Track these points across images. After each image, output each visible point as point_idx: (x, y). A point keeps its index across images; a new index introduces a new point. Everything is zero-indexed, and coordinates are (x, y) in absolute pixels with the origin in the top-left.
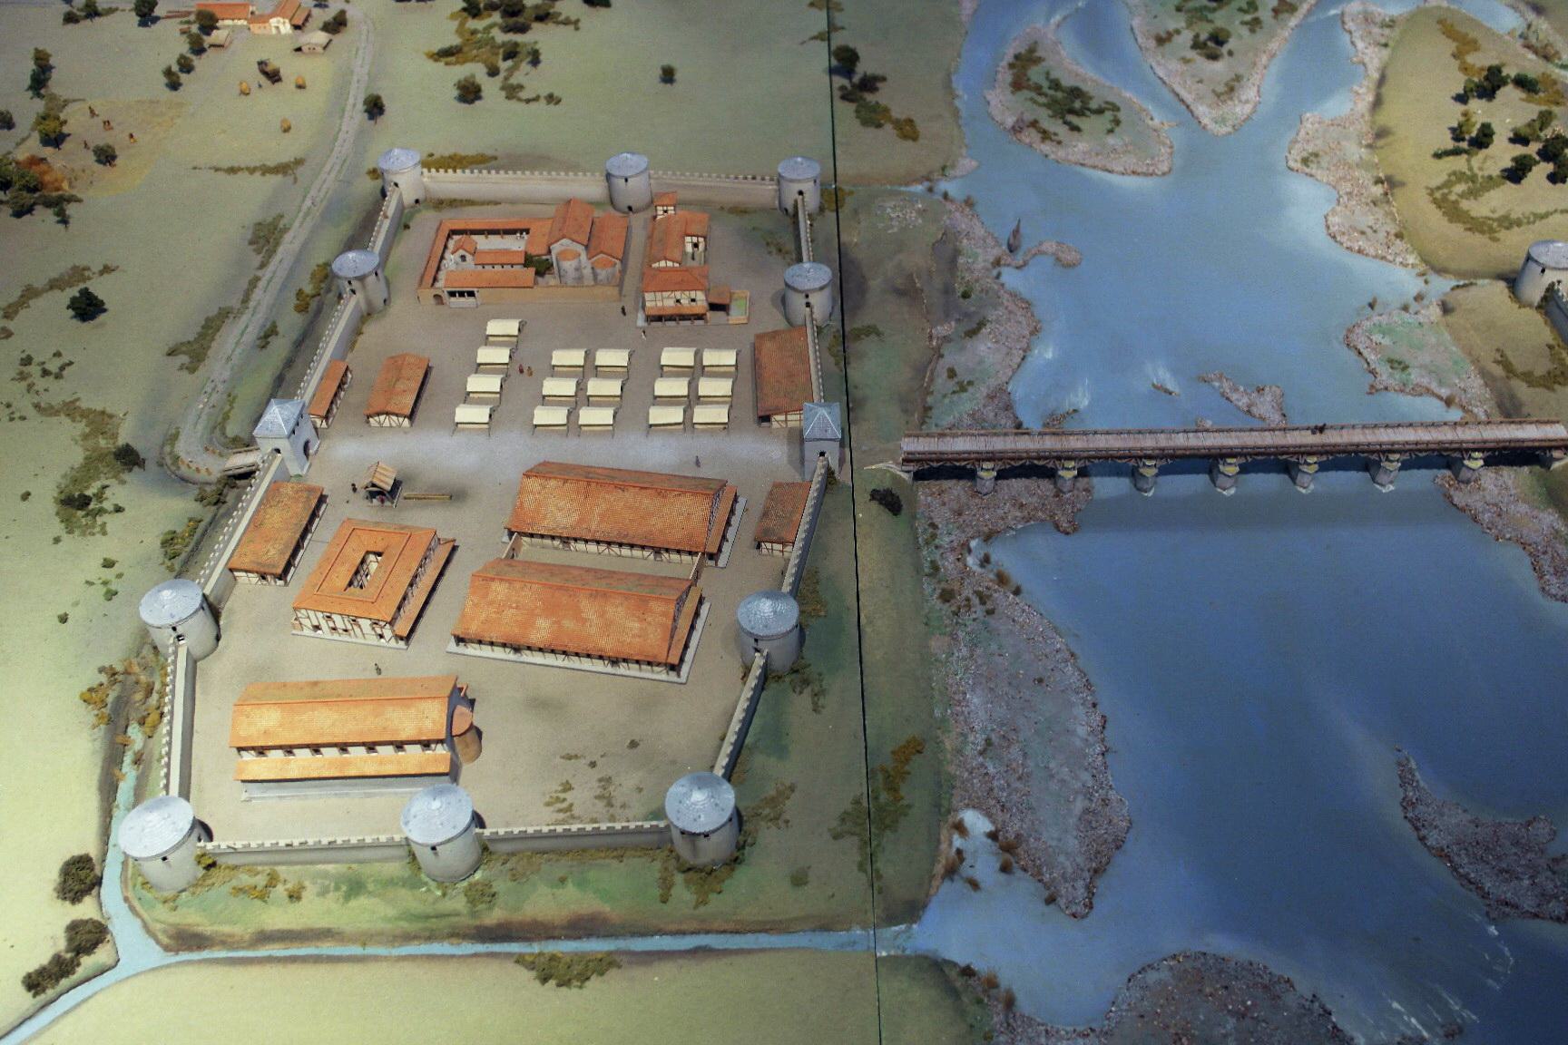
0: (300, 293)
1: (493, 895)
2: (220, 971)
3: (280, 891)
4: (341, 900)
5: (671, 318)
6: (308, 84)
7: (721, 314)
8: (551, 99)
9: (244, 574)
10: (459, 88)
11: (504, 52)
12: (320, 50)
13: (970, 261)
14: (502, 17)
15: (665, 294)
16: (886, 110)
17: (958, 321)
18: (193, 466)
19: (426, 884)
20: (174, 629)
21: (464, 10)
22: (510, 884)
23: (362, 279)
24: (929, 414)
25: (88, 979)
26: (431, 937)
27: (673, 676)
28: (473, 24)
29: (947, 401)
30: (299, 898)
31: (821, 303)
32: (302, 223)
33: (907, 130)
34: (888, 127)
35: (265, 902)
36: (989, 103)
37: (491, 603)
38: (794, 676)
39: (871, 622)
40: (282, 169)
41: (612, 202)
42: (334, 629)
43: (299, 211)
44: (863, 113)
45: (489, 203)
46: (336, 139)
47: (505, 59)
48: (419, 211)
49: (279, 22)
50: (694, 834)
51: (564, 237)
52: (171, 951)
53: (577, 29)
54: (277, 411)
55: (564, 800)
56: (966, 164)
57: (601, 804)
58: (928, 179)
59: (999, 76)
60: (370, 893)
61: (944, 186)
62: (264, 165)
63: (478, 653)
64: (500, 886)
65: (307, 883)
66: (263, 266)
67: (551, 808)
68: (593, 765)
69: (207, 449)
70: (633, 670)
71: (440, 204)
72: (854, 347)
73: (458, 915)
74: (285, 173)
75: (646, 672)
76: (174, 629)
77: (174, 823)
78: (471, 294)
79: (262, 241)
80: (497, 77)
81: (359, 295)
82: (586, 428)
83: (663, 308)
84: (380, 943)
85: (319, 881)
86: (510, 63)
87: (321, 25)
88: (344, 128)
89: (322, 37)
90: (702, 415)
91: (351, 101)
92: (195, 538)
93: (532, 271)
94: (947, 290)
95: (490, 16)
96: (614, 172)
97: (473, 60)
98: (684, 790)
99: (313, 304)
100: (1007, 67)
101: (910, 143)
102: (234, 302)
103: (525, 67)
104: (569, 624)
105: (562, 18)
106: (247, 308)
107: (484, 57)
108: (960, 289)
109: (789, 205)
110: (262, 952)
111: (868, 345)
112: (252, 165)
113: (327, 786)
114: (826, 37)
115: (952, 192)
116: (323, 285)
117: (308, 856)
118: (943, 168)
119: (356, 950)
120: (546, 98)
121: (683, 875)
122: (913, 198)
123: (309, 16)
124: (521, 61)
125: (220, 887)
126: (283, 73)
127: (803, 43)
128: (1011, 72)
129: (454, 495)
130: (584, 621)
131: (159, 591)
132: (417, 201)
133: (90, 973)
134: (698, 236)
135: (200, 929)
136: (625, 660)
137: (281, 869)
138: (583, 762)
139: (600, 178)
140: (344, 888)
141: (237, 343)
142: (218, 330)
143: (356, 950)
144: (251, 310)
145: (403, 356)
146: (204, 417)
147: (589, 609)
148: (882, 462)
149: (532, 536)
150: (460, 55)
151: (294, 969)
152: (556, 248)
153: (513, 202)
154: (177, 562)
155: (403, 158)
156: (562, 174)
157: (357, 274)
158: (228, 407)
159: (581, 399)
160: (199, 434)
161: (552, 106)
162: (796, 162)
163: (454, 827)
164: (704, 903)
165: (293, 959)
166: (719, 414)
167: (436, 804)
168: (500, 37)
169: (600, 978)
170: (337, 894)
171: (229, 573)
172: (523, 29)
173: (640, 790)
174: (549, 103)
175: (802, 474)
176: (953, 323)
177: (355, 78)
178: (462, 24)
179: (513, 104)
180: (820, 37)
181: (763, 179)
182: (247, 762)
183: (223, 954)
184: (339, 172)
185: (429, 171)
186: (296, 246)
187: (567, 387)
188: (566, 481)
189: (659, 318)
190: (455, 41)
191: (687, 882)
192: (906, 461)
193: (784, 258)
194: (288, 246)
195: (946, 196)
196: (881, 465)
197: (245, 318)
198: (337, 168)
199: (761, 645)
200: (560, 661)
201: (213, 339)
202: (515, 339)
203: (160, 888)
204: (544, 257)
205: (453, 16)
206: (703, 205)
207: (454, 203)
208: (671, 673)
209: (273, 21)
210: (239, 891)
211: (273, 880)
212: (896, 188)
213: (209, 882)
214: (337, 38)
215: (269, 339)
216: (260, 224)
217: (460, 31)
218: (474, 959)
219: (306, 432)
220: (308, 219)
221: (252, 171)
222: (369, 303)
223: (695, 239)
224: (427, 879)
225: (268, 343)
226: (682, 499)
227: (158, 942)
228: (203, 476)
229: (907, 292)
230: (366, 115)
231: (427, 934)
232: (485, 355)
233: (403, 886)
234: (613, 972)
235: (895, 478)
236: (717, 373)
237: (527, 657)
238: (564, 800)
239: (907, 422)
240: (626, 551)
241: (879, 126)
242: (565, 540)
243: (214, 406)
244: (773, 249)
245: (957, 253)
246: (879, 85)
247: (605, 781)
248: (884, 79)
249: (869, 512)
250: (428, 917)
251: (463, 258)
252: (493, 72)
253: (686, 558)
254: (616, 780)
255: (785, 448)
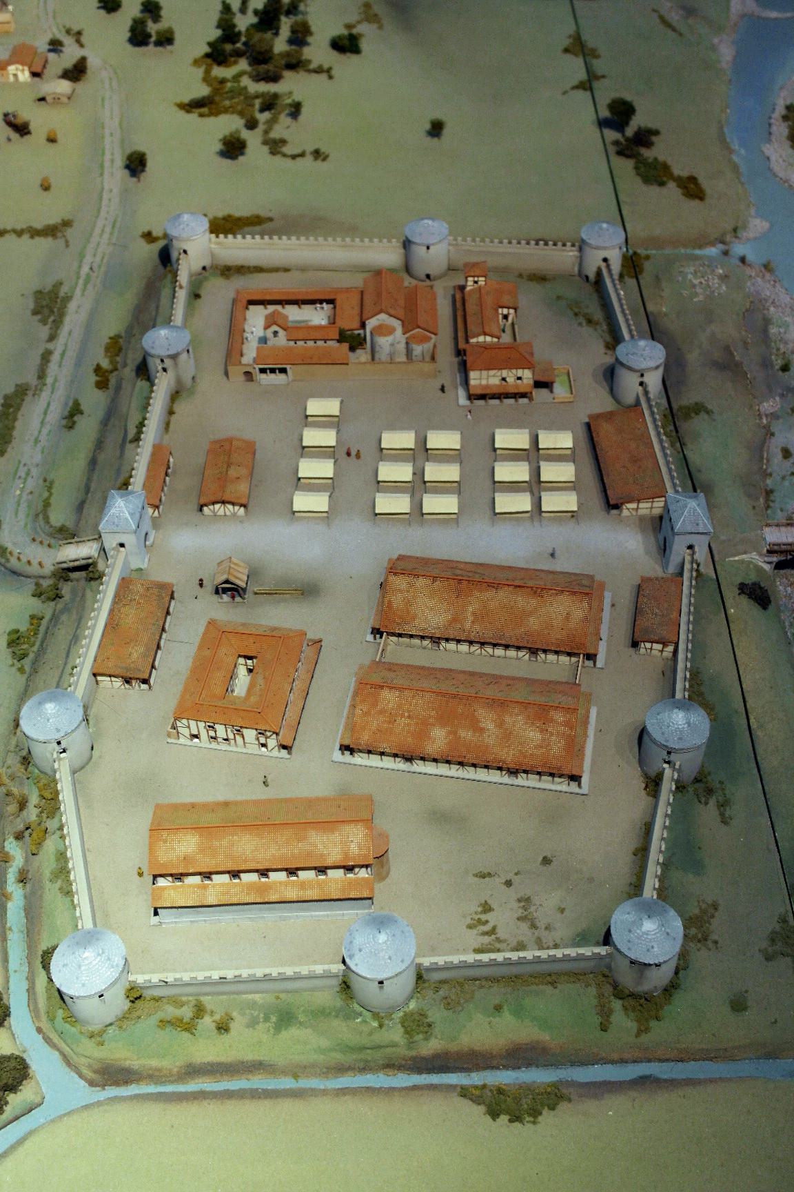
0: (98, 369)
1: (430, 1026)
2: (157, 1109)
3: (207, 1022)
4: (272, 1031)
5: (494, 396)
6: (59, 137)
7: (544, 392)
8: (317, 154)
9: (108, 679)
10: (225, 144)
11: (262, 104)
12: (65, 100)
13: (782, 330)
14: (250, 65)
15: (492, 372)
16: (666, 167)
17: (782, 396)
18: (24, 559)
19: (360, 1014)
20: (59, 743)
21: (207, 55)
22: (446, 1013)
23: (174, 357)
24: (772, 498)
25: (16, 1118)
26: (365, 1068)
27: (573, 787)
28: (219, 72)
29: (786, 483)
30: (227, 1030)
31: (654, 381)
32: (84, 290)
33: (692, 189)
34: (672, 185)
35: (193, 1034)
36: (768, 158)
37: (381, 712)
38: (697, 785)
39: (762, 726)
40: (51, 231)
41: (407, 268)
42: (215, 738)
43: (78, 278)
44: (642, 169)
45: (276, 270)
46: (101, 198)
47: (262, 110)
48: (206, 279)
49: (17, 69)
50: (645, 964)
51: (381, 311)
52: (96, 1085)
53: (331, 77)
54: (122, 504)
55: (487, 922)
56: (757, 226)
57: (524, 926)
58: (723, 242)
59: (774, 129)
60: (301, 1023)
61: (739, 249)
62: (31, 227)
63: (380, 764)
64: (436, 1015)
65: (235, 1014)
66: (52, 338)
67: (475, 931)
68: (509, 883)
69: (34, 540)
70: (532, 781)
71: (227, 271)
72: (684, 426)
73: (395, 1045)
74: (54, 236)
75: (546, 783)
76: (59, 743)
77: (109, 959)
78: (283, 371)
79: (46, 311)
80: (256, 130)
81: (171, 373)
82: (429, 517)
83: (487, 386)
84: (315, 1075)
85: (247, 1011)
86: (266, 115)
87: (60, 72)
88: (106, 186)
89: (65, 86)
90: (552, 502)
91: (108, 156)
92: (40, 636)
93: (346, 346)
94: (766, 364)
95: (235, 63)
96: (416, 239)
97: (226, 111)
98: (630, 918)
99: (113, 381)
100: (781, 120)
101: (696, 202)
102: (31, 379)
103: (284, 120)
104: (466, 734)
105: (312, 66)
106: (45, 385)
107: (239, 108)
108: (779, 363)
109: (591, 272)
110: (192, 1086)
111: (698, 424)
112: (18, 227)
113: (243, 911)
114: (586, 85)
115: (750, 257)
116: (118, 359)
117: (241, 987)
118: (735, 230)
119: (287, 1083)
120: (311, 153)
121: (620, 1002)
122: (711, 263)
123: (46, 61)
124: (279, 113)
125: (146, 1026)
126: (32, 127)
127: (565, 93)
128: (786, 124)
129: (306, 591)
130: (482, 730)
131: (40, 703)
132: (204, 268)
133: (18, 1112)
134: (509, 308)
135: (127, 1063)
136: (525, 772)
137: (206, 1000)
138: (498, 881)
139: (396, 244)
140: (274, 1019)
141: (42, 423)
142: (19, 409)
143: (287, 1083)
144: (49, 386)
145: (230, 441)
146: (24, 505)
147: (488, 720)
148: (745, 553)
149: (400, 635)
150: (213, 106)
151: (231, 1106)
152: (371, 323)
153: (303, 269)
154: (27, 663)
155: (193, 224)
156: (357, 240)
157: (172, 352)
158: (46, 494)
159: (419, 486)
160: (22, 523)
161: (319, 162)
162: (601, 228)
163: (402, 961)
164: (647, 1030)
165: (228, 1095)
166: (568, 501)
167: (382, 938)
168: (255, 87)
169: (552, 1113)
170: (268, 1024)
171: (93, 677)
172: (275, 78)
173: (562, 911)
174: (316, 159)
175: (665, 566)
176: (777, 398)
177: (107, 132)
178: (207, 72)
179: (278, 159)
180: (581, 86)
181: (564, 245)
182: (163, 889)
183: (152, 1089)
184: (111, 234)
185: (217, 237)
186: (83, 316)
187: (403, 472)
188: (435, 578)
189: (483, 397)
190: (203, 91)
191: (625, 1008)
192: (770, 552)
193: (596, 330)
194: (75, 317)
195: (743, 260)
196: (744, 556)
197: (45, 395)
198: (108, 230)
199: (673, 757)
200: (454, 771)
201: (15, 419)
202: (336, 419)
203: (84, 1022)
204: (356, 332)
205: (196, 63)
206: (503, 271)
207: (241, 270)
208: (572, 783)
209: (12, 69)
210: (164, 1023)
211: (200, 1010)
212: (689, 251)
213: (135, 1014)
214: (79, 86)
215: (75, 418)
216: (40, 292)
217: (207, 79)
218: (417, 1093)
219: (147, 525)
220: (89, 287)
221: (19, 233)
222: (179, 381)
223: (505, 311)
224: (359, 1009)
225: (74, 423)
226: (560, 598)
227: (81, 1076)
228: (34, 570)
229: (728, 365)
230: (127, 172)
231: (362, 1065)
232: (313, 437)
233: (337, 1017)
234: (563, 1106)
235: (759, 570)
236: (557, 456)
237: (419, 767)
238: (487, 922)
239: (754, 507)
240: (499, 652)
241: (662, 184)
242: (436, 640)
243: (31, 493)
244: (581, 319)
245: (767, 322)
246: (654, 139)
247: (526, 901)
248: (657, 133)
249: (740, 607)
250: (363, 1048)
251: (275, 333)
252: (251, 125)
253: (564, 659)
254: (536, 900)
255: (639, 537)
